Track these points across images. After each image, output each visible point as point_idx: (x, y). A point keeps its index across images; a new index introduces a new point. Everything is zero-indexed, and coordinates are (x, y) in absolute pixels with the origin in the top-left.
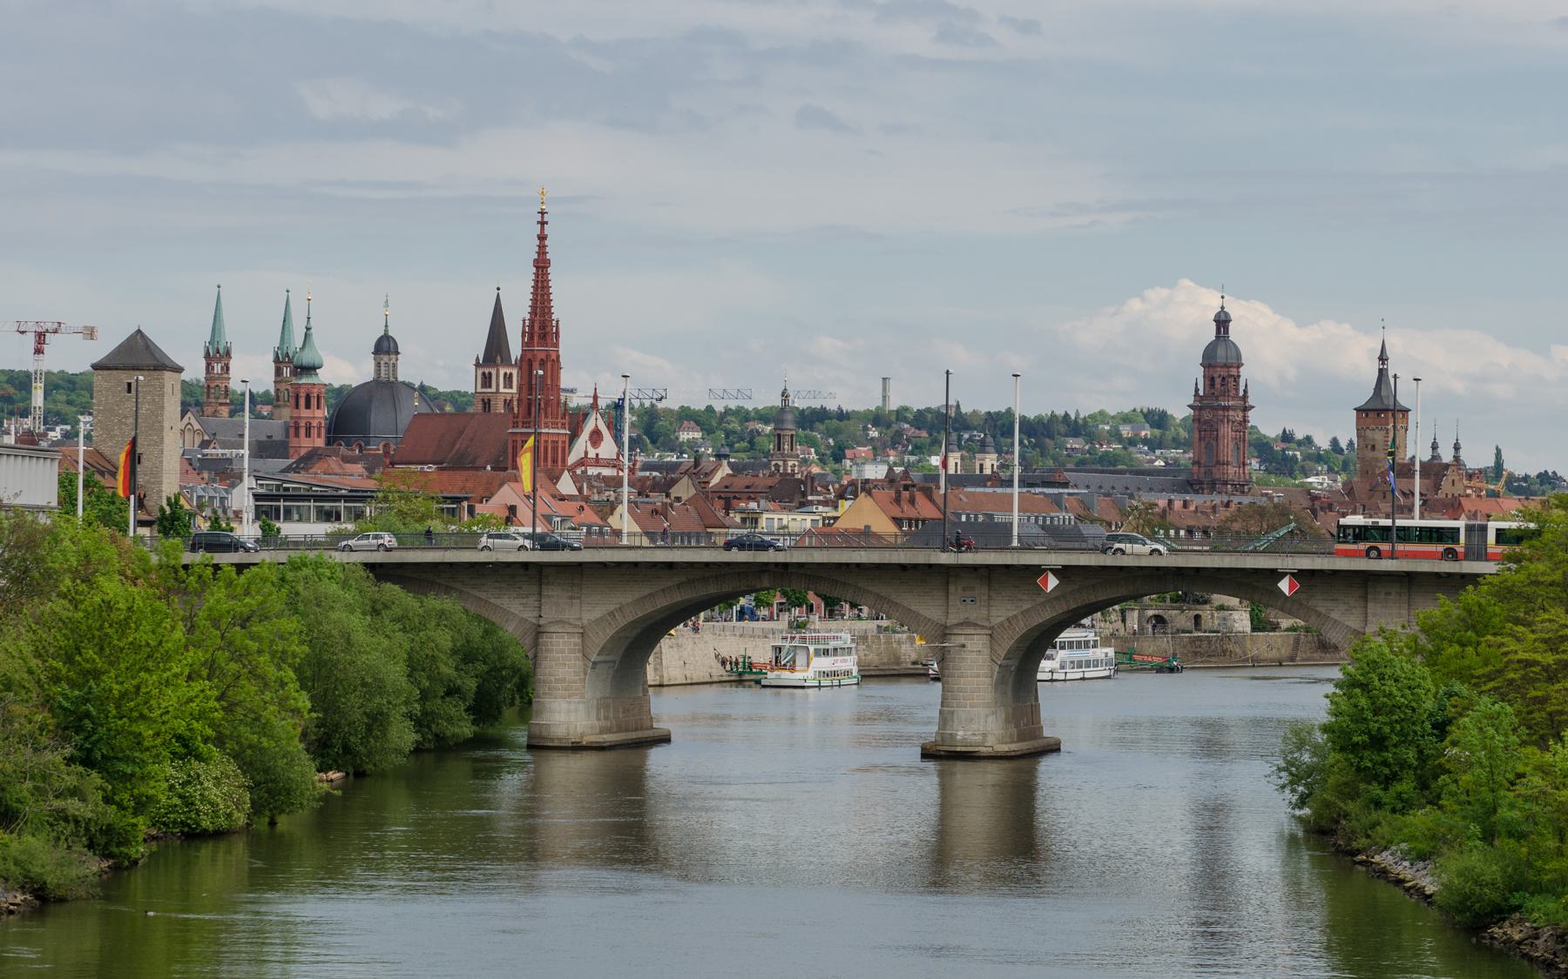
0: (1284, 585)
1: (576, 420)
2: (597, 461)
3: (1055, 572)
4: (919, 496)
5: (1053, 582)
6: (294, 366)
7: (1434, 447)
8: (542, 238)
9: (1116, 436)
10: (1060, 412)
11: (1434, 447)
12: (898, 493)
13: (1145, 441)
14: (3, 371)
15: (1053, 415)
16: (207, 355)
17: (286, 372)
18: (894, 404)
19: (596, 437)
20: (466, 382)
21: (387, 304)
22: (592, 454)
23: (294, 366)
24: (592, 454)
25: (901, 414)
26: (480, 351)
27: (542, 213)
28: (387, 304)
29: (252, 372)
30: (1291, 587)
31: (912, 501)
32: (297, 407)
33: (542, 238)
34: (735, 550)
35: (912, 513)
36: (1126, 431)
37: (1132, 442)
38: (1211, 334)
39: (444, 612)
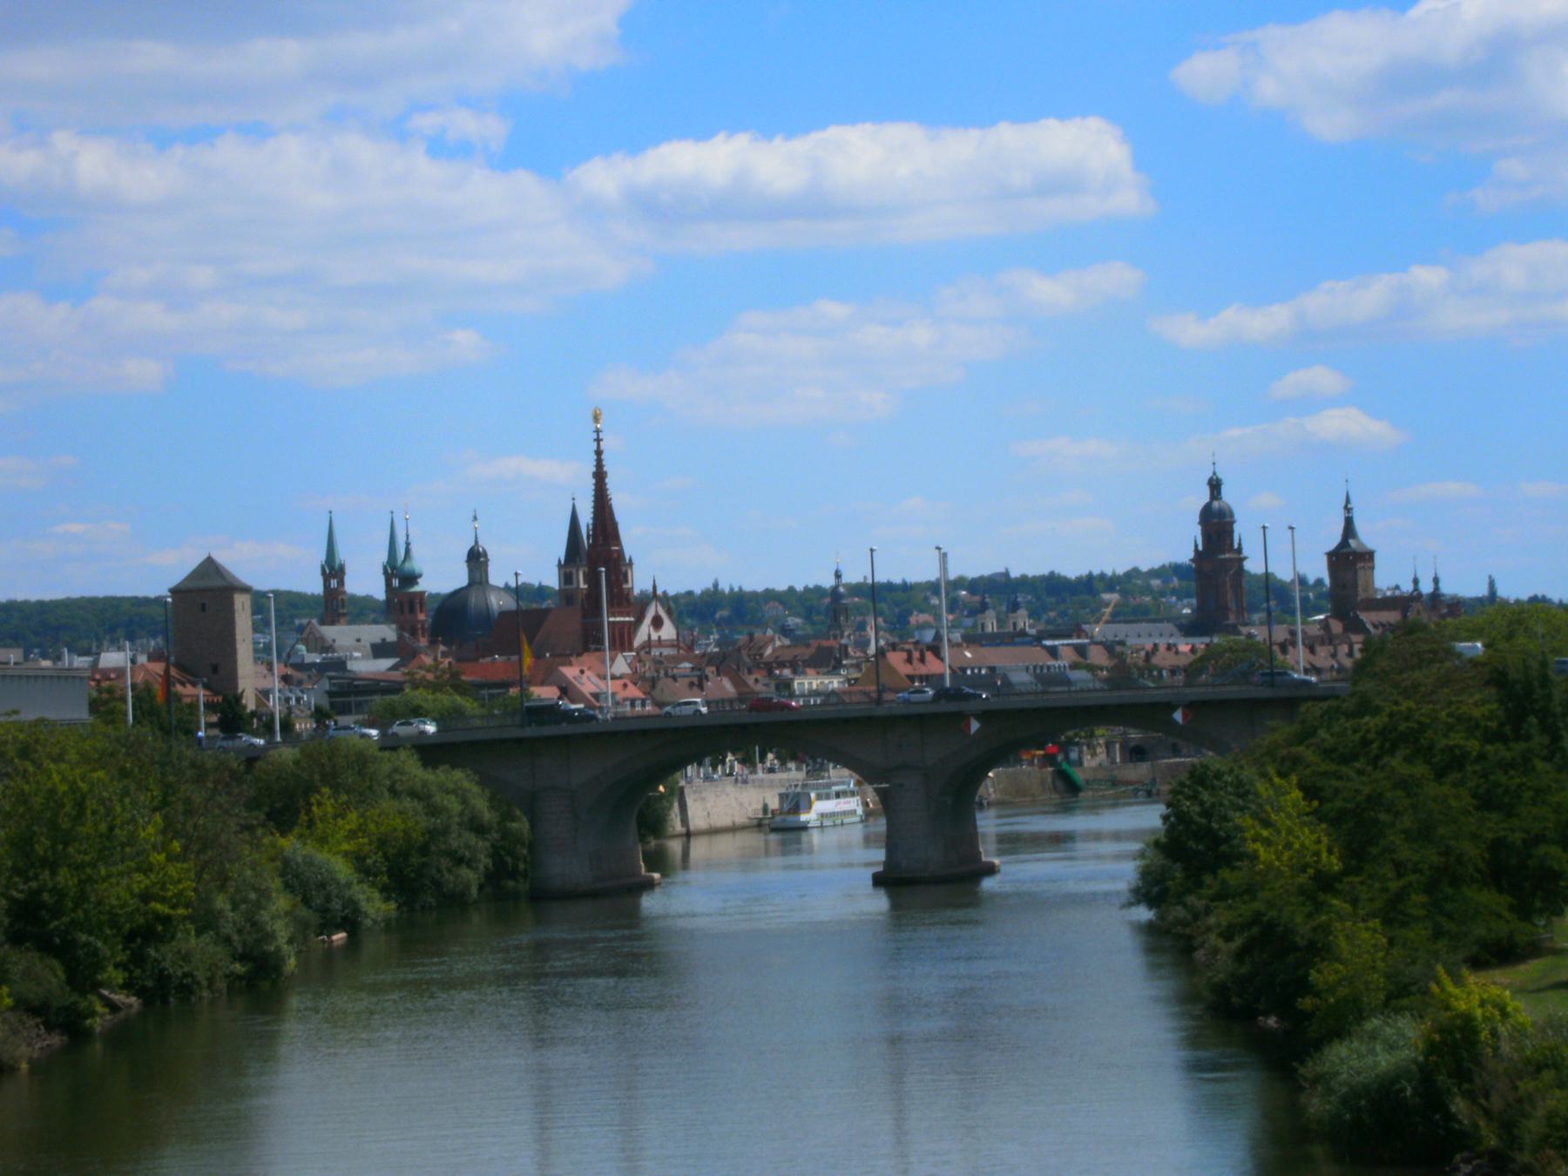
0: (1178, 716)
1: (638, 606)
2: (660, 642)
3: (978, 717)
4: (929, 656)
5: (975, 726)
6: (400, 576)
7: (1416, 581)
8: (599, 453)
9: (1148, 590)
10: (1096, 572)
11: (1416, 581)
12: (909, 653)
13: (1174, 592)
14: (10, 608)
15: (791, 589)
16: (323, 573)
17: (396, 583)
18: (952, 576)
19: (657, 623)
20: (552, 580)
21: (475, 518)
22: (654, 636)
23: (400, 576)
24: (654, 636)
25: (960, 583)
26: (561, 551)
27: (598, 431)
28: (475, 518)
29: (366, 581)
30: (1185, 716)
31: (922, 660)
32: (402, 612)
33: (599, 453)
34: (943, 702)
35: (923, 670)
36: (1156, 583)
37: (1162, 594)
38: (1204, 497)
39: (501, 780)
